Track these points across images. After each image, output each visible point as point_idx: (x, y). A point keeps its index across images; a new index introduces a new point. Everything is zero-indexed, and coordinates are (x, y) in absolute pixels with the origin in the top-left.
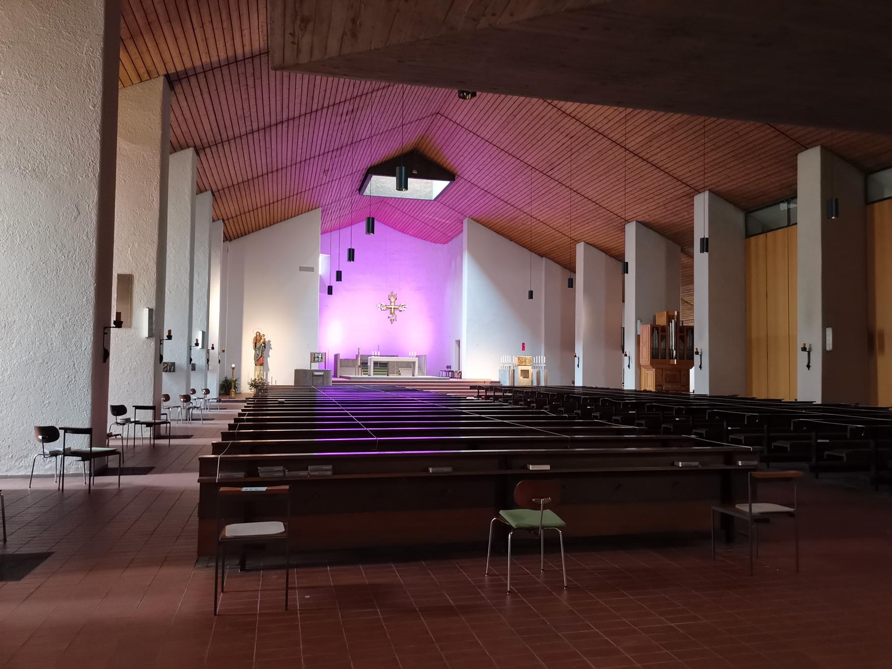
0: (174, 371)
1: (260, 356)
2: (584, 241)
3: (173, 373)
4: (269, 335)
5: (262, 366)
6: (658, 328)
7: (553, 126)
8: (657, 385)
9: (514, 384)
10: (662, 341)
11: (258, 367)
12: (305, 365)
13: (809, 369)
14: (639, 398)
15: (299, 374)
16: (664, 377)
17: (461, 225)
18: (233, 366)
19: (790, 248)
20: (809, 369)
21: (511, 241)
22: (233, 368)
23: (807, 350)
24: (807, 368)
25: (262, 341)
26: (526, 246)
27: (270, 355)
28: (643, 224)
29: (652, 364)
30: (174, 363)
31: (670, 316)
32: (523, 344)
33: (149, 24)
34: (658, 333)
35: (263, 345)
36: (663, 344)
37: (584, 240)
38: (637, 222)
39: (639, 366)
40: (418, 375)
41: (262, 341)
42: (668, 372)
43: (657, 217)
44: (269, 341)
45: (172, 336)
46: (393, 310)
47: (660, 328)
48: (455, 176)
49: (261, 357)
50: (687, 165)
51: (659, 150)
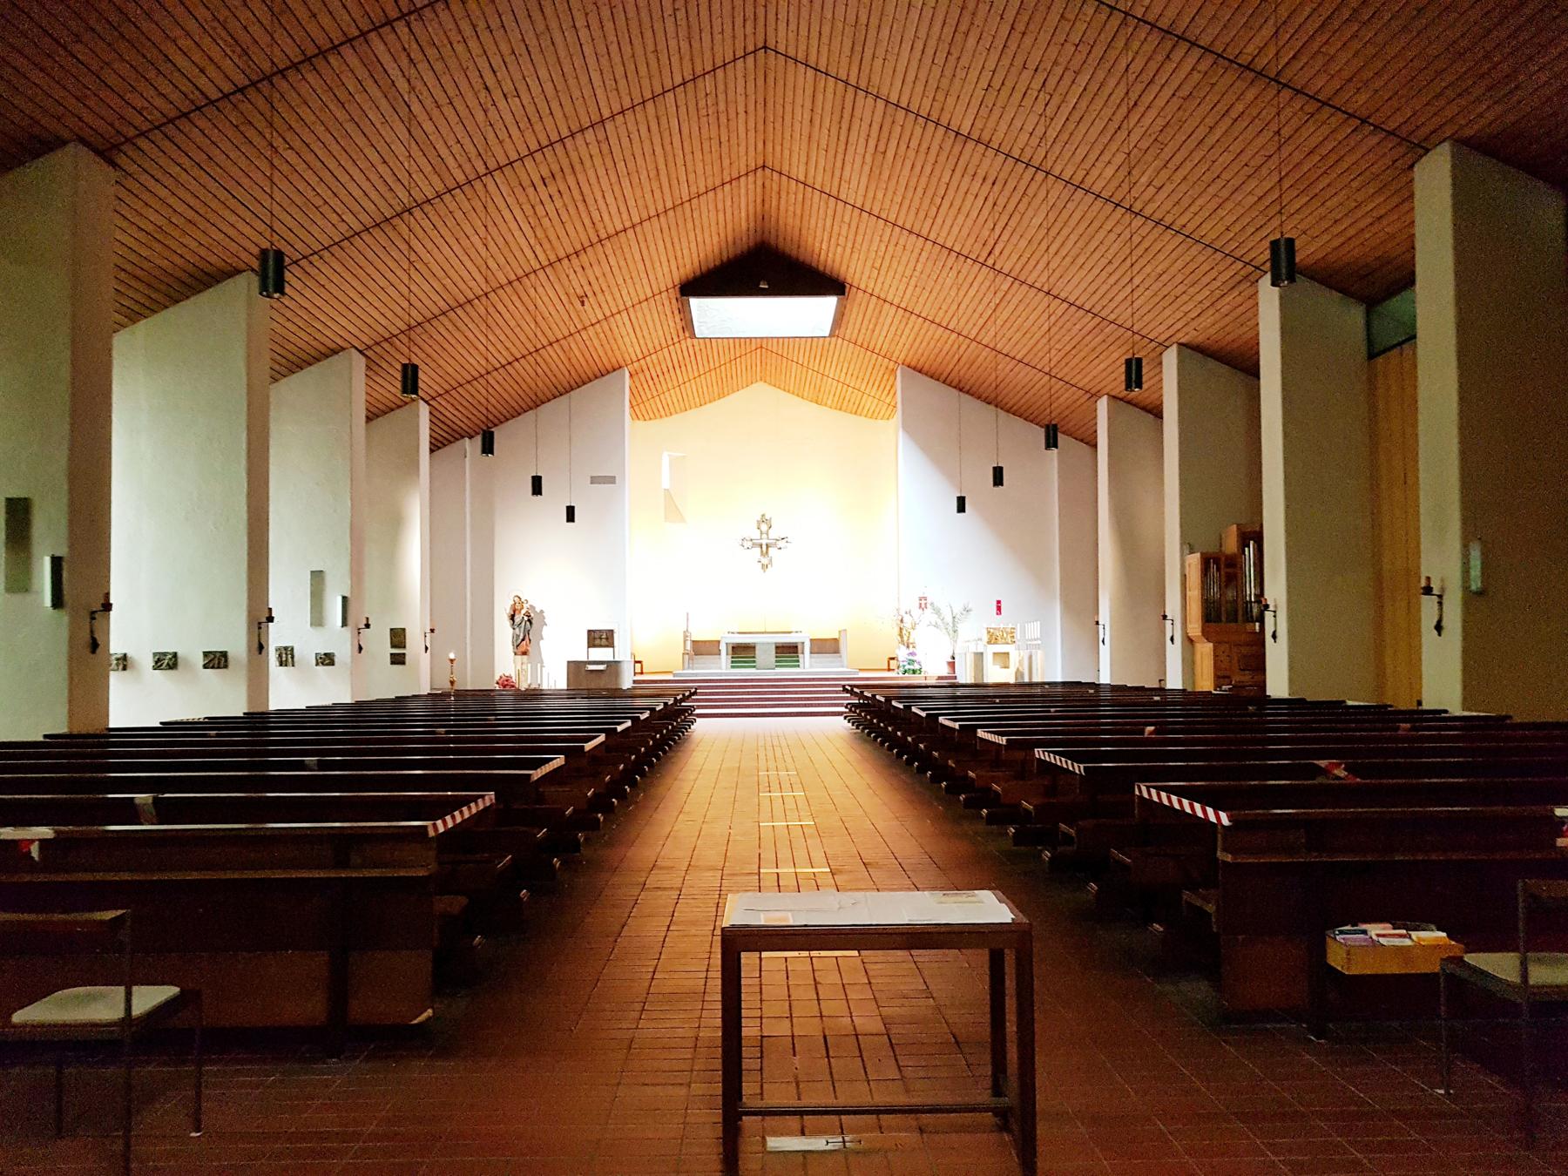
0: (226, 667)
1: (521, 637)
2: (1107, 394)
3: (224, 670)
4: (536, 599)
5: (525, 657)
6: (1220, 559)
7: (954, 163)
8: (1220, 678)
9: (1380, 688)
10: (1226, 586)
11: (519, 657)
12: (581, 652)
13: (1440, 635)
14: (1188, 698)
15: (575, 668)
16: (1235, 661)
17: (1157, 370)
18: (452, 656)
19: (1409, 376)
20: (1440, 635)
21: (989, 403)
22: (452, 661)
23: (1435, 592)
24: (1436, 632)
25: (523, 612)
26: (1016, 411)
27: (544, 636)
28: (1191, 350)
29: (1206, 634)
30: (226, 652)
31: (1244, 533)
32: (999, 602)
33: (973, 14)
34: (1218, 569)
35: (526, 618)
36: (1230, 594)
37: (1105, 391)
38: (1180, 344)
39: (1189, 641)
40: (811, 666)
41: (523, 612)
42: (1244, 650)
43: (1212, 331)
44: (542, 611)
45: (111, 605)
46: (764, 547)
47: (1223, 559)
48: (844, 287)
49: (523, 640)
50: (1216, 218)
51: (1152, 190)
